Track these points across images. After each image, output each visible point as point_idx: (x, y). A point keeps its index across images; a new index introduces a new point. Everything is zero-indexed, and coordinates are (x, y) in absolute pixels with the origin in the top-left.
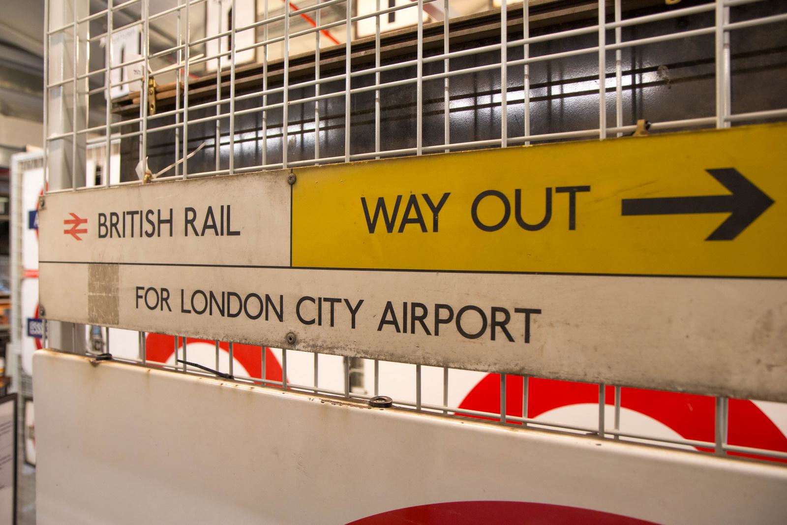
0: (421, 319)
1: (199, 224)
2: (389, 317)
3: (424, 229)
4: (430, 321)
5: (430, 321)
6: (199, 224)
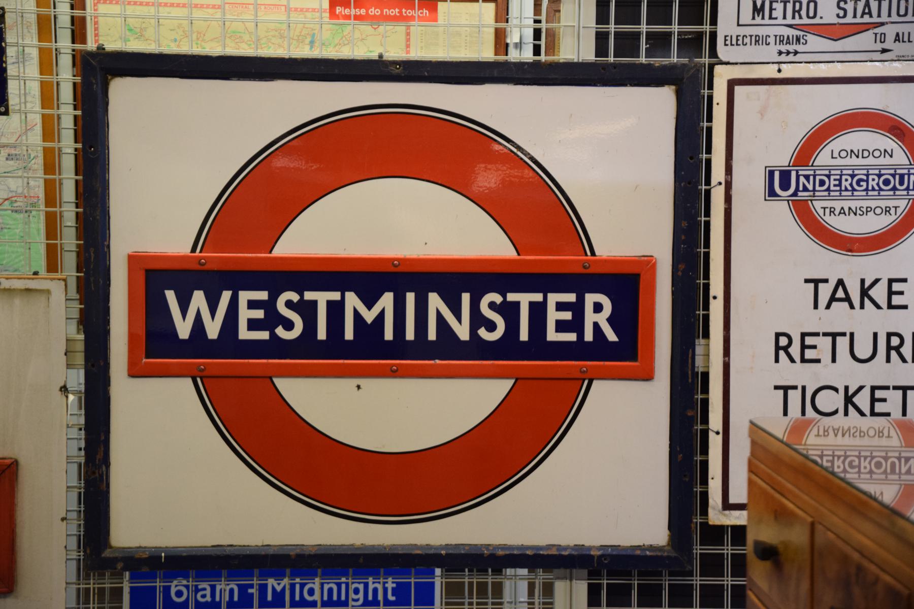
0: (786, 349)
1: (837, 212)
2: (840, 294)
3: (852, 307)
4: (795, 350)
5: (795, 350)
6: (837, 212)
